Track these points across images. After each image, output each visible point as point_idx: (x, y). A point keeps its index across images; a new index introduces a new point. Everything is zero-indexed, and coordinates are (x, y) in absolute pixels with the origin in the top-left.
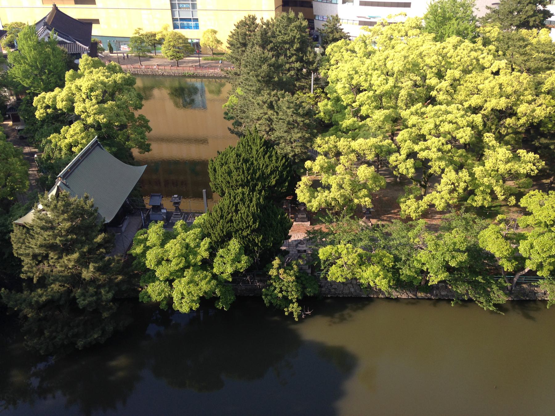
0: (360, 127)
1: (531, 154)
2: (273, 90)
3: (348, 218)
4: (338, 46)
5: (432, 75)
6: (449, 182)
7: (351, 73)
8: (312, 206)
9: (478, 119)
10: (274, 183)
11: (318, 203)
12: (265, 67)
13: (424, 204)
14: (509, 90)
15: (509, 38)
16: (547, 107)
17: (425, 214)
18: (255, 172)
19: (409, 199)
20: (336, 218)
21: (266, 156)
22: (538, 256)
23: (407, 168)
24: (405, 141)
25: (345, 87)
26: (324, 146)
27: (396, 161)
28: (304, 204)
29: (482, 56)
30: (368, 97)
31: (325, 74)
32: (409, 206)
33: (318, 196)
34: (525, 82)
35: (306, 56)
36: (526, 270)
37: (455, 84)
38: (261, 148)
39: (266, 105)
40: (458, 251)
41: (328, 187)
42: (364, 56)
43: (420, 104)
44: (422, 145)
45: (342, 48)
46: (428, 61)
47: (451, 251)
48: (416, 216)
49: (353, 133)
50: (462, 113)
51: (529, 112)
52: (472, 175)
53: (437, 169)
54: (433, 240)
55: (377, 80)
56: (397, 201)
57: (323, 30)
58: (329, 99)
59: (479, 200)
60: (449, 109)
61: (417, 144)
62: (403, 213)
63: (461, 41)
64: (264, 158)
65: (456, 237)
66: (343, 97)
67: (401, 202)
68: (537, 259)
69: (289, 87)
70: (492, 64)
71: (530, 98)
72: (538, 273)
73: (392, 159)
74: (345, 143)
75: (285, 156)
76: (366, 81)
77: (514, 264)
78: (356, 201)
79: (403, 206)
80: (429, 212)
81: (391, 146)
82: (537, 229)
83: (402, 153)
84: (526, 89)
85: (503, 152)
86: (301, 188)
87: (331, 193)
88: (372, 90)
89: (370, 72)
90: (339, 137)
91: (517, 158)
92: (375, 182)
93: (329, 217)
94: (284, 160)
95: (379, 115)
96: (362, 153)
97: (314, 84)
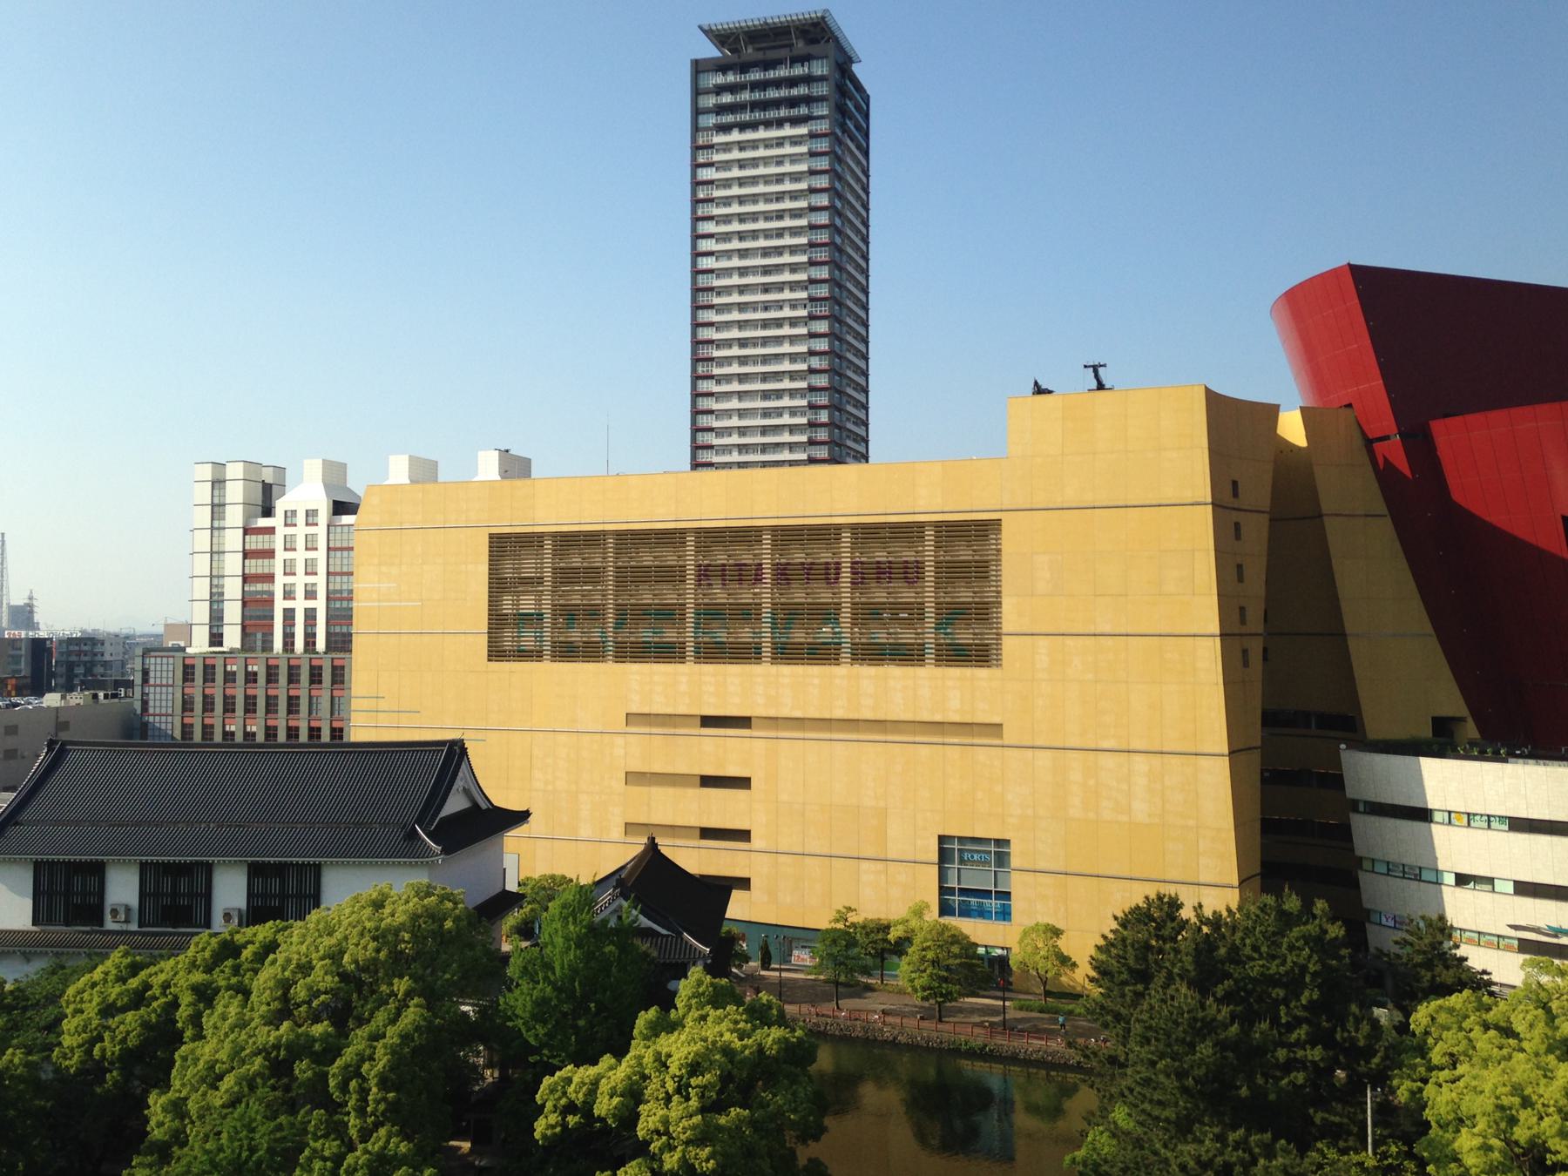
4: (1451, 1011)
7: (1506, 1101)
12: (1205, 1049)
31: (1413, 1093)
35: (1344, 1029)
42: (1550, 1050)
45: (1466, 1017)
57: (1398, 956)
97: (1374, 1125)
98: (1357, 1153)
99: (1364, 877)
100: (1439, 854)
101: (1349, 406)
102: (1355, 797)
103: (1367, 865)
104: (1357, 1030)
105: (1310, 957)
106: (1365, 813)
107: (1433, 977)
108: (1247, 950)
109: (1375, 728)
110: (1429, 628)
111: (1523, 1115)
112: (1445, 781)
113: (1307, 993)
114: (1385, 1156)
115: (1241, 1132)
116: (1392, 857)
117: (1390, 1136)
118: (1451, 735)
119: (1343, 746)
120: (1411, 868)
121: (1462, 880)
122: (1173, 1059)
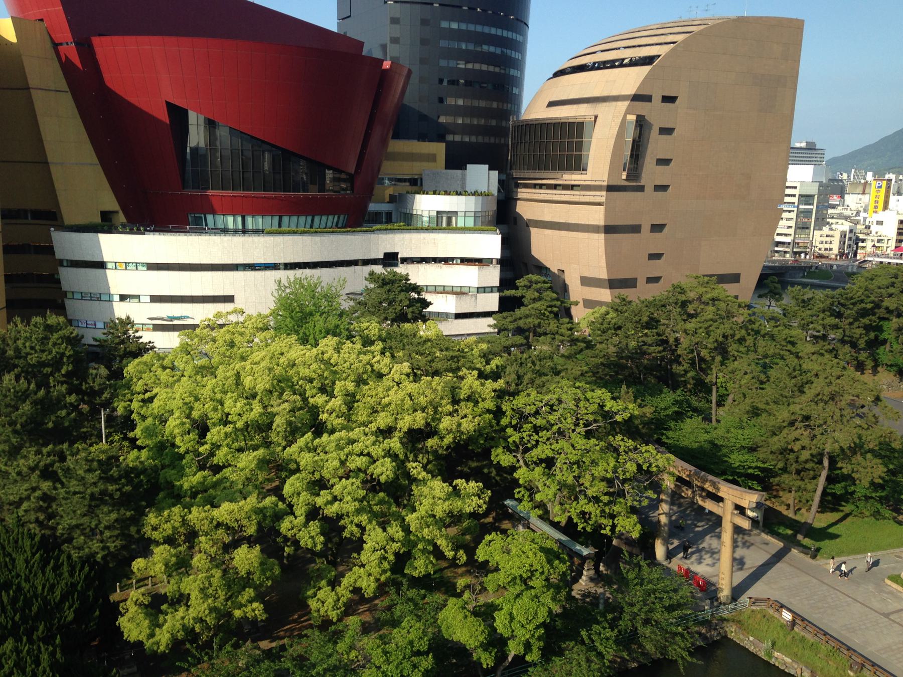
0: (215, 485)
1: (472, 484)
2: (45, 445)
3: (228, 647)
4: (145, 364)
5: (315, 391)
6: (377, 546)
7: (187, 400)
8: (158, 643)
9: (395, 443)
10: (71, 617)
11: (168, 635)
12: (26, 407)
13: (344, 591)
14: (422, 400)
15: (402, 335)
16: (474, 418)
17: (349, 609)
18: (28, 603)
19: (320, 589)
20: (207, 654)
21: (48, 569)
22: (523, 631)
23: (311, 536)
24: (299, 494)
25: (183, 424)
26: (165, 526)
27: (292, 529)
28: (140, 644)
29: (375, 360)
30: (226, 434)
31: (125, 408)
32: (324, 601)
33: (165, 621)
34: (439, 388)
35: (86, 383)
36: (510, 659)
37: (351, 400)
38: (34, 555)
39: (38, 472)
40: (418, 653)
41: (182, 599)
42: (197, 373)
43: (309, 435)
44: (325, 496)
45: (153, 365)
46: (305, 372)
47: (410, 657)
48: (338, 615)
49: (208, 495)
50: (373, 438)
51: (454, 426)
52: (406, 529)
53: (355, 529)
54: (378, 647)
55: (233, 405)
56: (300, 596)
57: (105, 341)
58: (140, 448)
59: (420, 566)
60: (352, 435)
61: (318, 495)
62: (315, 614)
63: (340, 342)
64: (44, 573)
65: (409, 632)
66: (178, 441)
67: (309, 597)
68: (523, 635)
69: (67, 434)
70: (391, 369)
71: (450, 408)
72: (528, 658)
73: (285, 526)
74: (203, 514)
75: (89, 560)
76: (215, 410)
77: (493, 654)
78: (237, 613)
79: (313, 604)
80: (358, 600)
81: (277, 505)
82: (511, 589)
83: (298, 513)
84: (442, 398)
85: (438, 487)
86: (129, 615)
87: (191, 610)
88: (230, 423)
89: (218, 396)
90: (188, 507)
91: (456, 492)
92: (263, 572)
93: (193, 656)
94: (87, 569)
95: (248, 460)
96: (235, 525)
97: (106, 428)
98: (97, 444)
99: (68, 303)
100: (111, 284)
101: (42, 20)
102: (61, 257)
103: (69, 295)
104: (94, 382)
105: (66, 348)
106: (67, 266)
107: (125, 349)
108: (28, 350)
109: (69, 218)
110: (96, 161)
111: (196, 405)
112: (113, 246)
113: (65, 368)
114: (112, 442)
115: (51, 447)
116: (84, 290)
117: (114, 431)
118: (110, 220)
119: (52, 229)
120: (86, 294)
121: (123, 298)
122: (6, 417)
